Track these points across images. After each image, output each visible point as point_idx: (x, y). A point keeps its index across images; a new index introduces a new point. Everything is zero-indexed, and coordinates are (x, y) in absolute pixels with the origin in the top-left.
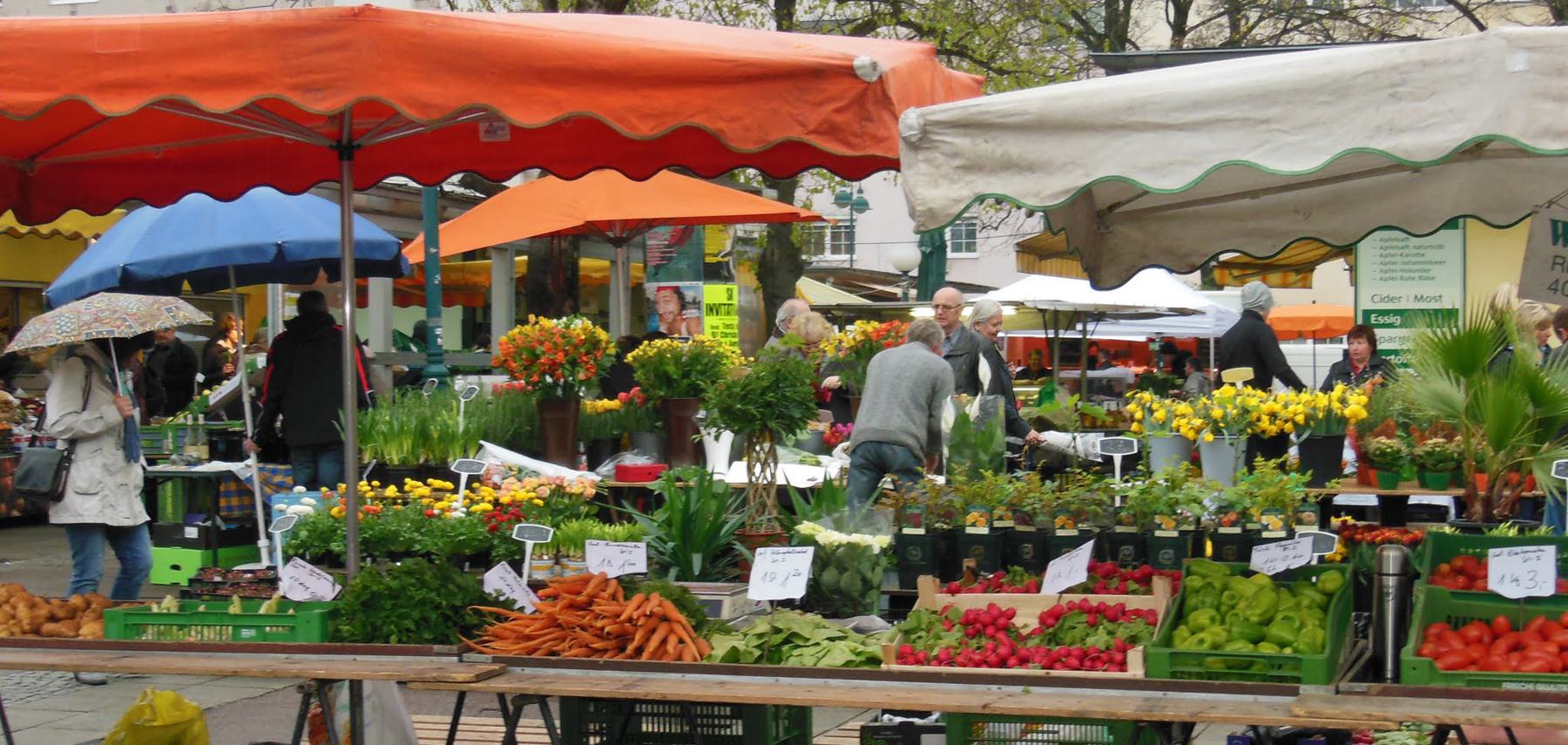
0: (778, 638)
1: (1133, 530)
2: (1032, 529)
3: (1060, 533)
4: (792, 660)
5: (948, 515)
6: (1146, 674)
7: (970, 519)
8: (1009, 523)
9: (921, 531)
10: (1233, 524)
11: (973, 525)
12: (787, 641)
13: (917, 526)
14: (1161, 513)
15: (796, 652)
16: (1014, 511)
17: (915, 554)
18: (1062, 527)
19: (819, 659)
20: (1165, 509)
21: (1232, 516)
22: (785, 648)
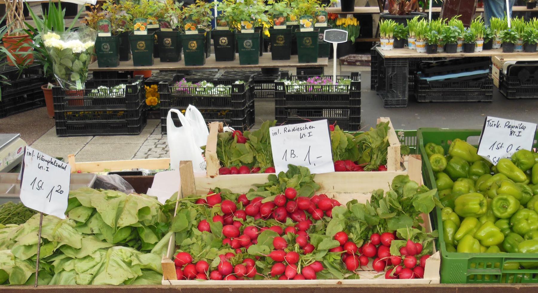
0: (47, 251)
1: (227, 28)
2: (171, 30)
3: (187, 33)
4: (65, 275)
5: (124, 23)
6: (441, 281)
7: (136, 26)
8: (157, 26)
9: (109, 35)
10: (282, 24)
11: (138, 30)
12: (58, 252)
13: (106, 31)
14: (245, 20)
15: (68, 265)
16: (159, 21)
17: (106, 47)
18: (189, 30)
19: (94, 277)
20: (248, 18)
21: (282, 19)
22: (57, 261)
